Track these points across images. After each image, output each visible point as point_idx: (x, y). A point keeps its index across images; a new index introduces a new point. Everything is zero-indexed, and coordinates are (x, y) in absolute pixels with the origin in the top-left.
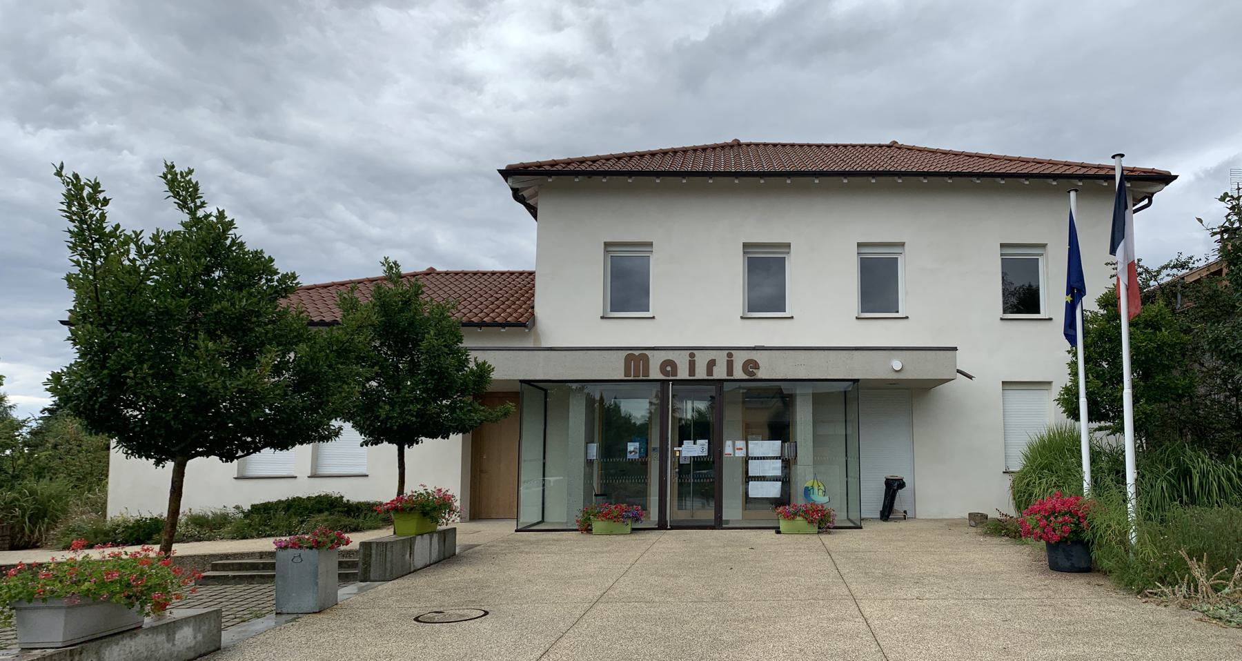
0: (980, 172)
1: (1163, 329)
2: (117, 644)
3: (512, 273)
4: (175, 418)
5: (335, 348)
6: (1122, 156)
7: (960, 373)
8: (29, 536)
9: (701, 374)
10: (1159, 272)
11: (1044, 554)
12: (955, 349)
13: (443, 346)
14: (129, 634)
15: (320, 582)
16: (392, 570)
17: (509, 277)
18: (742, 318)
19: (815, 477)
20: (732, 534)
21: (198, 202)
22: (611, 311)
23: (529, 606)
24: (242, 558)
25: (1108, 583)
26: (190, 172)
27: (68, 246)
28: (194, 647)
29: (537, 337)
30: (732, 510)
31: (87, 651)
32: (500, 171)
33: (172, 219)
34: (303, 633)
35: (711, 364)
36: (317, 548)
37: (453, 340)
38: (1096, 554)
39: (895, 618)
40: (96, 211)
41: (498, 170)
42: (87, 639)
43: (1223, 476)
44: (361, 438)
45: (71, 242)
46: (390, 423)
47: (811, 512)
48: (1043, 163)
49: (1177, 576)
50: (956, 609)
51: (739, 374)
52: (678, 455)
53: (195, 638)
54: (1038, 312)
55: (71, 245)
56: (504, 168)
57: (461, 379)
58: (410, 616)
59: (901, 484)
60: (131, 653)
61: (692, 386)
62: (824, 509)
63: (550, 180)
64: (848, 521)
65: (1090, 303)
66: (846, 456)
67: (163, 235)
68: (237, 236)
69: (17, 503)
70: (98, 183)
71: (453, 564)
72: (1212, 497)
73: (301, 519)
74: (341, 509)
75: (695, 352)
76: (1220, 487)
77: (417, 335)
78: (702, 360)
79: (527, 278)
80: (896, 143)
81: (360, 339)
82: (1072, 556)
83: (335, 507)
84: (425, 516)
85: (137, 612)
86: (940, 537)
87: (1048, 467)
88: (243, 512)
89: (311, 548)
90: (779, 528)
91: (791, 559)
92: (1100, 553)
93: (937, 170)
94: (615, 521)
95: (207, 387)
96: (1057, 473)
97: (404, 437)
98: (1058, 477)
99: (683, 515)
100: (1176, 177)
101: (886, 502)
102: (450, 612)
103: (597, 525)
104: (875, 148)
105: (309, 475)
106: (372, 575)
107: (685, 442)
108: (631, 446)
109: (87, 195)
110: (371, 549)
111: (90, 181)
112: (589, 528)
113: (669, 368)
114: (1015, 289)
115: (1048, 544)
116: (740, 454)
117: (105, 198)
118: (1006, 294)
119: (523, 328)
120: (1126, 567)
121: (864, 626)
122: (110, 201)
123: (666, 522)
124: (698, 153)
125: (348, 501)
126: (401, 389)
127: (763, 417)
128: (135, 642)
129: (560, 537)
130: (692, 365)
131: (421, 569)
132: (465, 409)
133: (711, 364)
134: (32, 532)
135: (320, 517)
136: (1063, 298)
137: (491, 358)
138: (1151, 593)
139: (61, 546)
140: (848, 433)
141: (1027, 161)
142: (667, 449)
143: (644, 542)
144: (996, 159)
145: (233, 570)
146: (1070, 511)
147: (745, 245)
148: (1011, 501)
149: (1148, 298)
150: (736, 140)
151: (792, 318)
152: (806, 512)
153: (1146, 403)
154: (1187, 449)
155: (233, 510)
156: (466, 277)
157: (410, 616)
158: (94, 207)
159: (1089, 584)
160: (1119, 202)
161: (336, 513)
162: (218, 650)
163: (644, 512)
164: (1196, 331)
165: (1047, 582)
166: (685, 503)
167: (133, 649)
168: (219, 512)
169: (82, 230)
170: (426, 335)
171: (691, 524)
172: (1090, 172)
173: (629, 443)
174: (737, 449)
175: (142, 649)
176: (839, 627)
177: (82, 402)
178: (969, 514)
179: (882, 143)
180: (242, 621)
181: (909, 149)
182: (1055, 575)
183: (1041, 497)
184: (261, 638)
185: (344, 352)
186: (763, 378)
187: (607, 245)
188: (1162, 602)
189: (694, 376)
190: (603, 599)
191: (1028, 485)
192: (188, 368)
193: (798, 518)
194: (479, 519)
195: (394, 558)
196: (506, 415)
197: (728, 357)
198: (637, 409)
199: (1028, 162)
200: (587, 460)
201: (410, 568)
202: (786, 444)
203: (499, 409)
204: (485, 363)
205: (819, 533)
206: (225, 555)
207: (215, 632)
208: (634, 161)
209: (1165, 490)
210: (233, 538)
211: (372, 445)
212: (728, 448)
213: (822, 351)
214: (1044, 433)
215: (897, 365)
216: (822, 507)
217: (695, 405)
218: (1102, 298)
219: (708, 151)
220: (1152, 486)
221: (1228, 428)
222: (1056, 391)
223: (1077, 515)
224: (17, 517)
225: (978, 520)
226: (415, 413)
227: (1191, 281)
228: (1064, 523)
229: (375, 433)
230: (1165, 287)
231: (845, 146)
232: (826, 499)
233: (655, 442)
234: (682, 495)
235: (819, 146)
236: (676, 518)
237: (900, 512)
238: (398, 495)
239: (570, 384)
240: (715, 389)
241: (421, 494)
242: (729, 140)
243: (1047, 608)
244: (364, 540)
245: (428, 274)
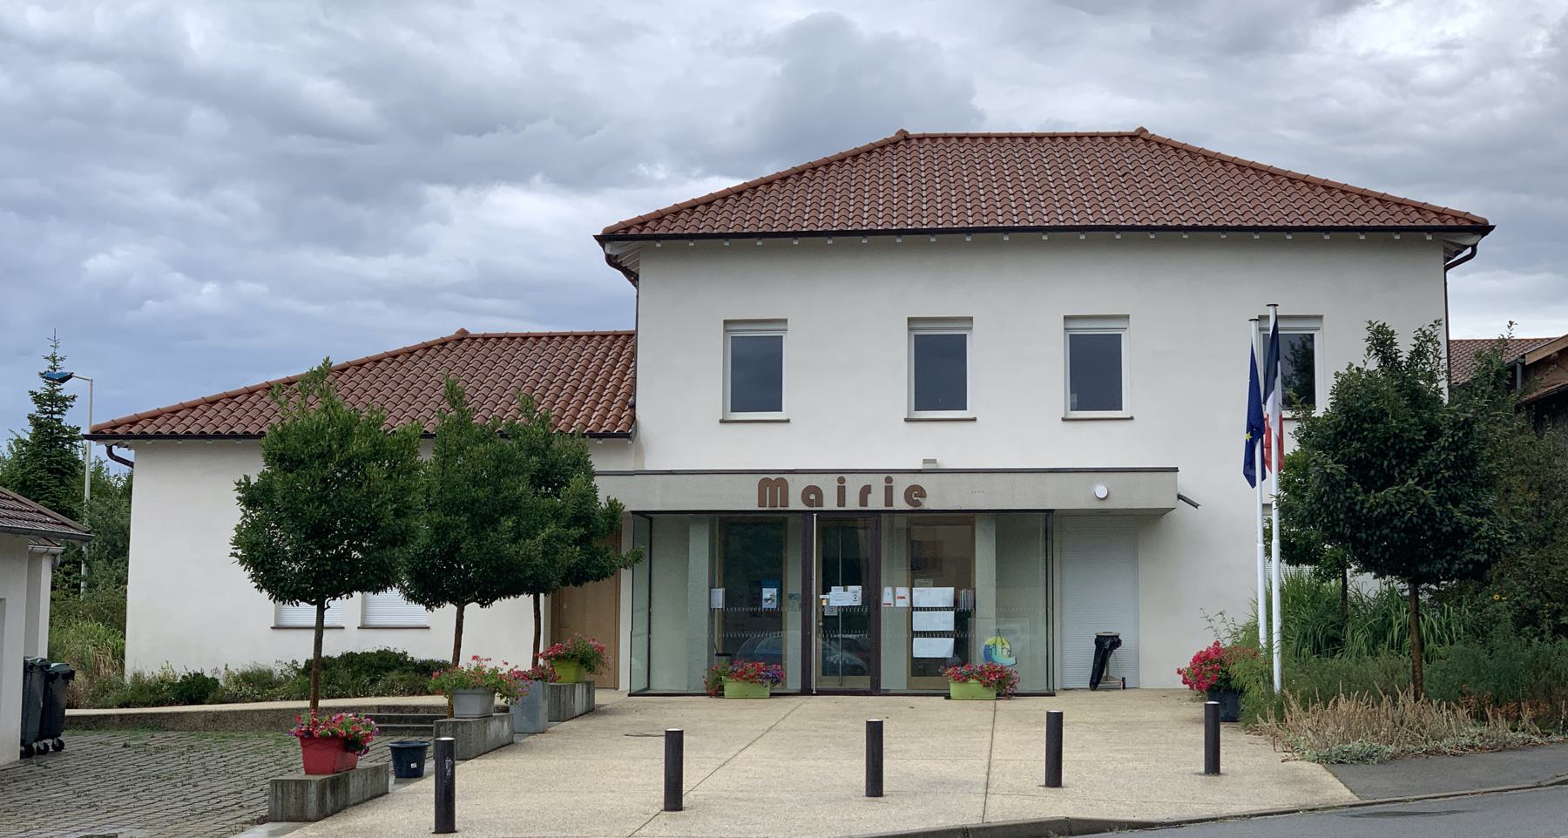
7: (1183, 500)
12: (1176, 470)
18: (907, 420)
22: (732, 411)
30: (893, 669)
32: (596, 237)
35: (866, 491)
47: (987, 673)
51: (900, 503)
52: (824, 604)
59: (1115, 642)
71: (513, 750)
78: (853, 486)
80: (1146, 131)
89: (536, 679)
103: (730, 687)
105: (359, 625)
113: (812, 497)
130: (841, 492)
133: (866, 491)
142: (811, 595)
152: (982, 673)
173: (764, 589)
174: (899, 598)
186: (932, 508)
189: (844, 506)
193: (972, 681)
200: (711, 609)
212: (887, 596)
215: (1101, 491)
236: (819, 687)
237: (1114, 679)
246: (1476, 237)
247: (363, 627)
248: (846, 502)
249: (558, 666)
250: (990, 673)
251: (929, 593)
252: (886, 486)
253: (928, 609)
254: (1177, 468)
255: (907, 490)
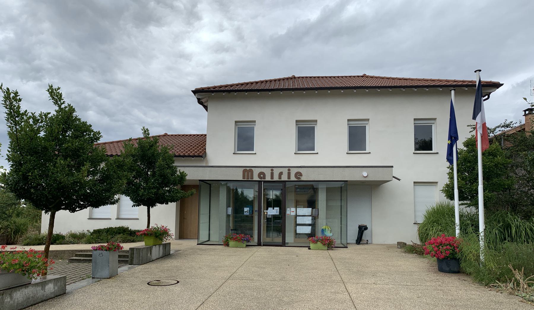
0: (405, 86)
1: (498, 156)
2: (19, 291)
3: (198, 135)
4: (49, 193)
5: (117, 164)
6: (480, 71)
8: (14, 240)
9: (276, 178)
10: (495, 129)
11: (435, 263)
12: (392, 167)
13: (166, 164)
14: (24, 286)
15: (110, 265)
16: (142, 260)
17: (196, 137)
18: (295, 153)
19: (327, 225)
20: (290, 249)
21: (62, 101)
22: (237, 151)
23: (198, 280)
24: (87, 252)
25: (469, 279)
26: (59, 88)
27: (6, 119)
28: (54, 292)
29: (207, 162)
30: (290, 238)
31: (5, 294)
32: (193, 91)
33: (52, 110)
34: (101, 287)
35: (281, 174)
36: (109, 251)
37: (170, 162)
38: (463, 265)
39: (363, 294)
40: (16, 104)
41: (192, 91)
42: (5, 288)
43: (528, 228)
44: (132, 203)
45: (6, 118)
46: (144, 197)
47: (324, 240)
48: (435, 81)
49: (507, 277)
50: (393, 290)
51: (293, 178)
53: (54, 288)
54: (431, 150)
55: (7, 119)
56: (194, 90)
57: (173, 179)
58: (146, 282)
59: (366, 228)
60: (26, 294)
61: (272, 184)
62: (331, 238)
63: (213, 94)
64: (341, 244)
65: (460, 145)
66: (341, 215)
67: (43, 114)
68: (77, 116)
69: (9, 227)
70: (17, 92)
71: (168, 258)
72: (522, 238)
73: (112, 236)
74: (128, 233)
75: (273, 169)
76: (526, 233)
77: (155, 160)
79: (204, 137)
80: (366, 75)
81: (128, 161)
82: (450, 265)
83: (125, 232)
84: (156, 237)
85: (27, 277)
86: (384, 253)
87: (437, 222)
88: (90, 233)
89: (106, 250)
90: (310, 247)
91: (315, 261)
92: (465, 265)
93: (385, 85)
94: (239, 242)
95: (61, 180)
96: (441, 224)
97: (150, 203)
98: (442, 226)
99: (268, 240)
100: (502, 85)
101: (359, 236)
102: (163, 281)
103: (231, 243)
104: (355, 77)
105: (116, 218)
106: (134, 262)
107: (269, 208)
108: (246, 209)
109: (12, 97)
110: (134, 251)
111: (14, 91)
112: (228, 244)
113: (262, 176)
114: (418, 141)
115: (438, 259)
116: (293, 214)
117: (20, 98)
118: (416, 143)
119: (201, 158)
120: (478, 272)
121: (348, 297)
122: (22, 100)
123: (261, 242)
124: (277, 82)
125: (131, 229)
126: (148, 183)
127: (305, 198)
128: (27, 290)
129: (215, 248)
130: (272, 174)
131: (155, 260)
132: (175, 192)
133: (281, 174)
134: (14, 238)
135: (119, 236)
136: (446, 142)
137: (186, 170)
138: (493, 286)
139: (23, 244)
140: (342, 205)
141: (427, 80)
142: (261, 211)
143: (251, 252)
144: (412, 80)
145: (83, 257)
146: (450, 244)
147: (297, 121)
148: (418, 238)
149: (491, 141)
150: (293, 75)
151: (318, 153)
152: (322, 240)
153: (488, 192)
154: (509, 215)
155: (86, 232)
156: (180, 137)
157: (146, 282)
158: (15, 102)
159: (459, 279)
160: (478, 93)
161: (125, 234)
162: (64, 294)
163: (251, 238)
164: (522, 155)
165: (438, 278)
166: (270, 234)
167: (26, 293)
168: (81, 232)
169: (11, 112)
170: (158, 160)
171: (272, 244)
172: (458, 84)
175: (30, 293)
176: (336, 297)
177: (13, 186)
178: (397, 242)
179: (359, 75)
180: (82, 279)
181: (371, 77)
182: (442, 274)
183: (433, 236)
184: (84, 289)
185: (120, 166)
186: (304, 180)
187: (236, 122)
188: (499, 290)
189: (273, 179)
190: (231, 278)
191: (426, 230)
192: (53, 172)
193: (319, 243)
194: (183, 238)
195: (143, 255)
196: (192, 195)
197: (288, 170)
198: (250, 194)
199: (428, 81)
200: (227, 214)
201: (150, 259)
202: (314, 210)
203: (189, 192)
204: (183, 172)
205: (328, 249)
206: (81, 250)
207: (63, 286)
208: (248, 86)
209: (497, 234)
210: (86, 243)
211: (137, 206)
212: (288, 212)
213: (331, 168)
214: (435, 206)
215: (365, 174)
216: (330, 238)
217: (274, 192)
218: (466, 142)
219: (281, 81)
220: (490, 232)
221: (529, 205)
222: (442, 185)
223: (454, 246)
224: (9, 232)
225: (402, 245)
226: (154, 193)
227: (511, 133)
228: (447, 250)
229: (138, 201)
230: (498, 136)
231: (342, 77)
232: (331, 234)
233: (256, 208)
234: (268, 229)
235: (330, 77)
237: (365, 240)
238: (147, 227)
239: (221, 182)
240: (282, 185)
241: (155, 228)
242: (290, 76)
243: (439, 291)
244: (131, 247)
245: (164, 136)
246: (495, 89)
247: (117, 219)
248: (274, 178)
249: (146, 238)
250: (325, 240)
251: (303, 210)
252: (288, 172)
253: (302, 216)
254: (393, 166)
255: (295, 173)
